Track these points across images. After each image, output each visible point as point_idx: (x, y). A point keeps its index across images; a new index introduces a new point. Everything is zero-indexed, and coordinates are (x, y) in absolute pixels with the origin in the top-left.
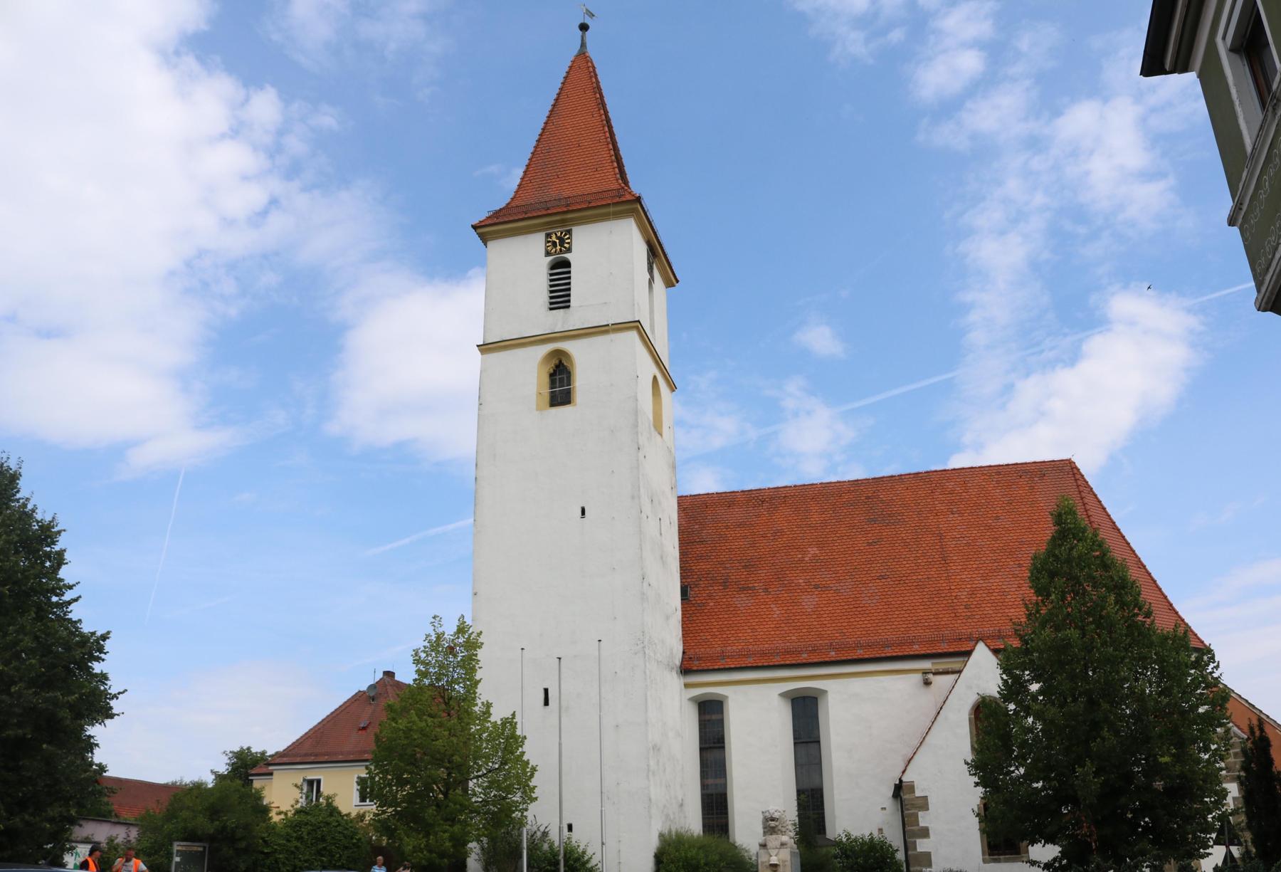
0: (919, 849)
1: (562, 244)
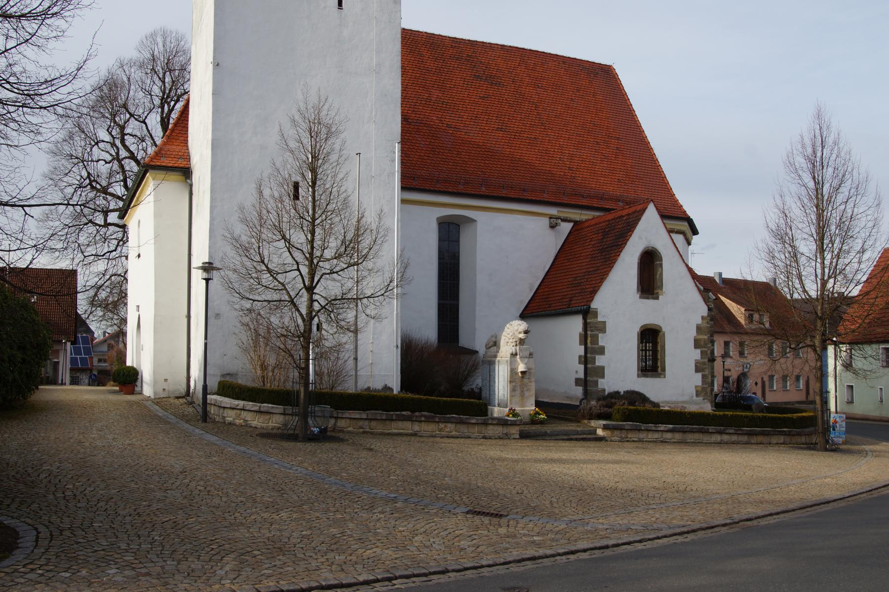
0: (597, 364)
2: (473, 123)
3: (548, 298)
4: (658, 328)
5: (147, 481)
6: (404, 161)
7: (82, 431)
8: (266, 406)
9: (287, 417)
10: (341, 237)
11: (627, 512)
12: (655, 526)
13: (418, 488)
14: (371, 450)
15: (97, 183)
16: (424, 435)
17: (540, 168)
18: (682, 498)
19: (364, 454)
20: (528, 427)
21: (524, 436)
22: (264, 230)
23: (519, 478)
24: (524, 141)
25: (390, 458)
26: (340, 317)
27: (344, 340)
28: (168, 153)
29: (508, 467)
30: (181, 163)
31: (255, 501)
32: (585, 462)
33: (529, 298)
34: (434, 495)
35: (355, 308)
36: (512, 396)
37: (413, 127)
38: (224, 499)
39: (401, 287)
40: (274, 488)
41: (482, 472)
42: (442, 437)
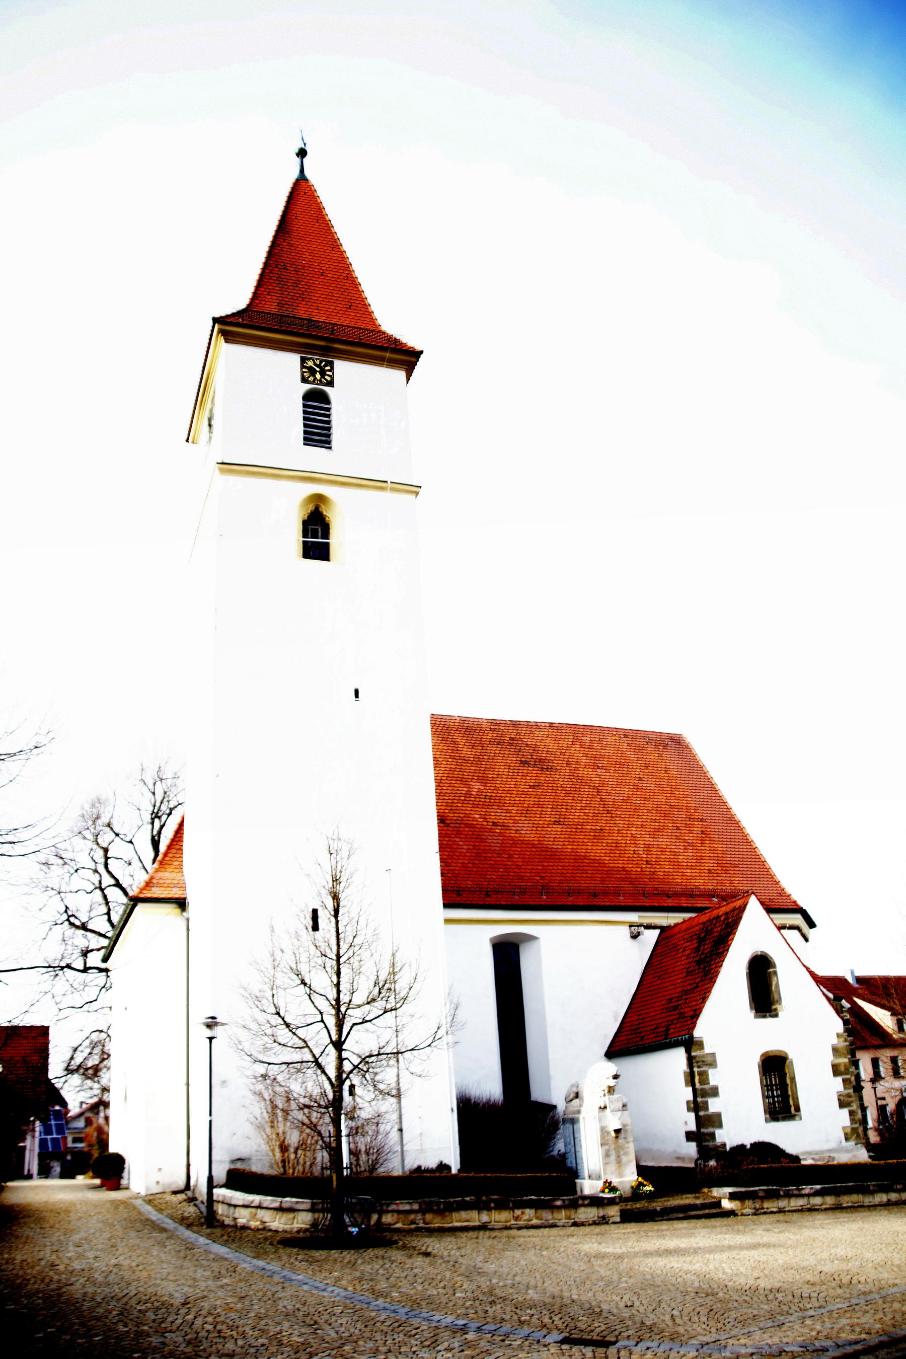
1: (323, 373)
2: (524, 819)
3: (638, 1028)
4: (783, 1055)
5: (139, 1320)
6: (445, 872)
7: (55, 1248)
8: (288, 1201)
9: (316, 1215)
10: (374, 978)
11: (776, 1324)
12: (818, 1344)
13: (494, 1308)
14: (427, 1254)
15: (76, 918)
16: (495, 1227)
17: (611, 865)
18: (848, 1296)
19: (419, 1261)
20: (631, 1205)
21: (627, 1217)
22: (279, 975)
23: (626, 1282)
24: (588, 834)
25: (454, 1266)
26: (378, 1078)
27: (383, 1109)
28: (161, 881)
29: (610, 1266)
30: (176, 893)
31: (280, 1343)
32: (711, 1250)
33: (615, 1030)
34: (515, 1317)
35: (396, 1064)
36: (606, 1164)
37: (452, 829)
38: (240, 1343)
39: (452, 1033)
40: (304, 1322)
41: (576, 1277)
42: (520, 1228)
